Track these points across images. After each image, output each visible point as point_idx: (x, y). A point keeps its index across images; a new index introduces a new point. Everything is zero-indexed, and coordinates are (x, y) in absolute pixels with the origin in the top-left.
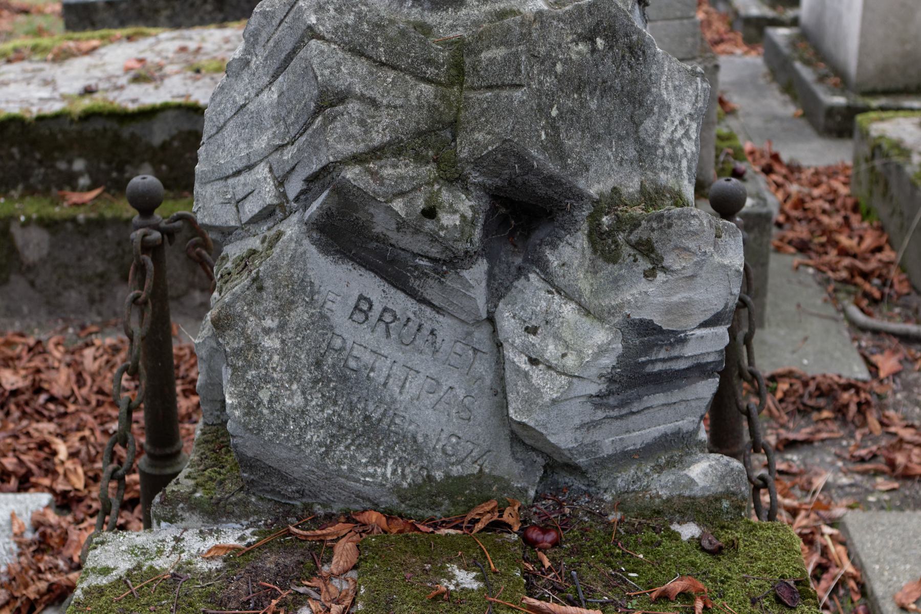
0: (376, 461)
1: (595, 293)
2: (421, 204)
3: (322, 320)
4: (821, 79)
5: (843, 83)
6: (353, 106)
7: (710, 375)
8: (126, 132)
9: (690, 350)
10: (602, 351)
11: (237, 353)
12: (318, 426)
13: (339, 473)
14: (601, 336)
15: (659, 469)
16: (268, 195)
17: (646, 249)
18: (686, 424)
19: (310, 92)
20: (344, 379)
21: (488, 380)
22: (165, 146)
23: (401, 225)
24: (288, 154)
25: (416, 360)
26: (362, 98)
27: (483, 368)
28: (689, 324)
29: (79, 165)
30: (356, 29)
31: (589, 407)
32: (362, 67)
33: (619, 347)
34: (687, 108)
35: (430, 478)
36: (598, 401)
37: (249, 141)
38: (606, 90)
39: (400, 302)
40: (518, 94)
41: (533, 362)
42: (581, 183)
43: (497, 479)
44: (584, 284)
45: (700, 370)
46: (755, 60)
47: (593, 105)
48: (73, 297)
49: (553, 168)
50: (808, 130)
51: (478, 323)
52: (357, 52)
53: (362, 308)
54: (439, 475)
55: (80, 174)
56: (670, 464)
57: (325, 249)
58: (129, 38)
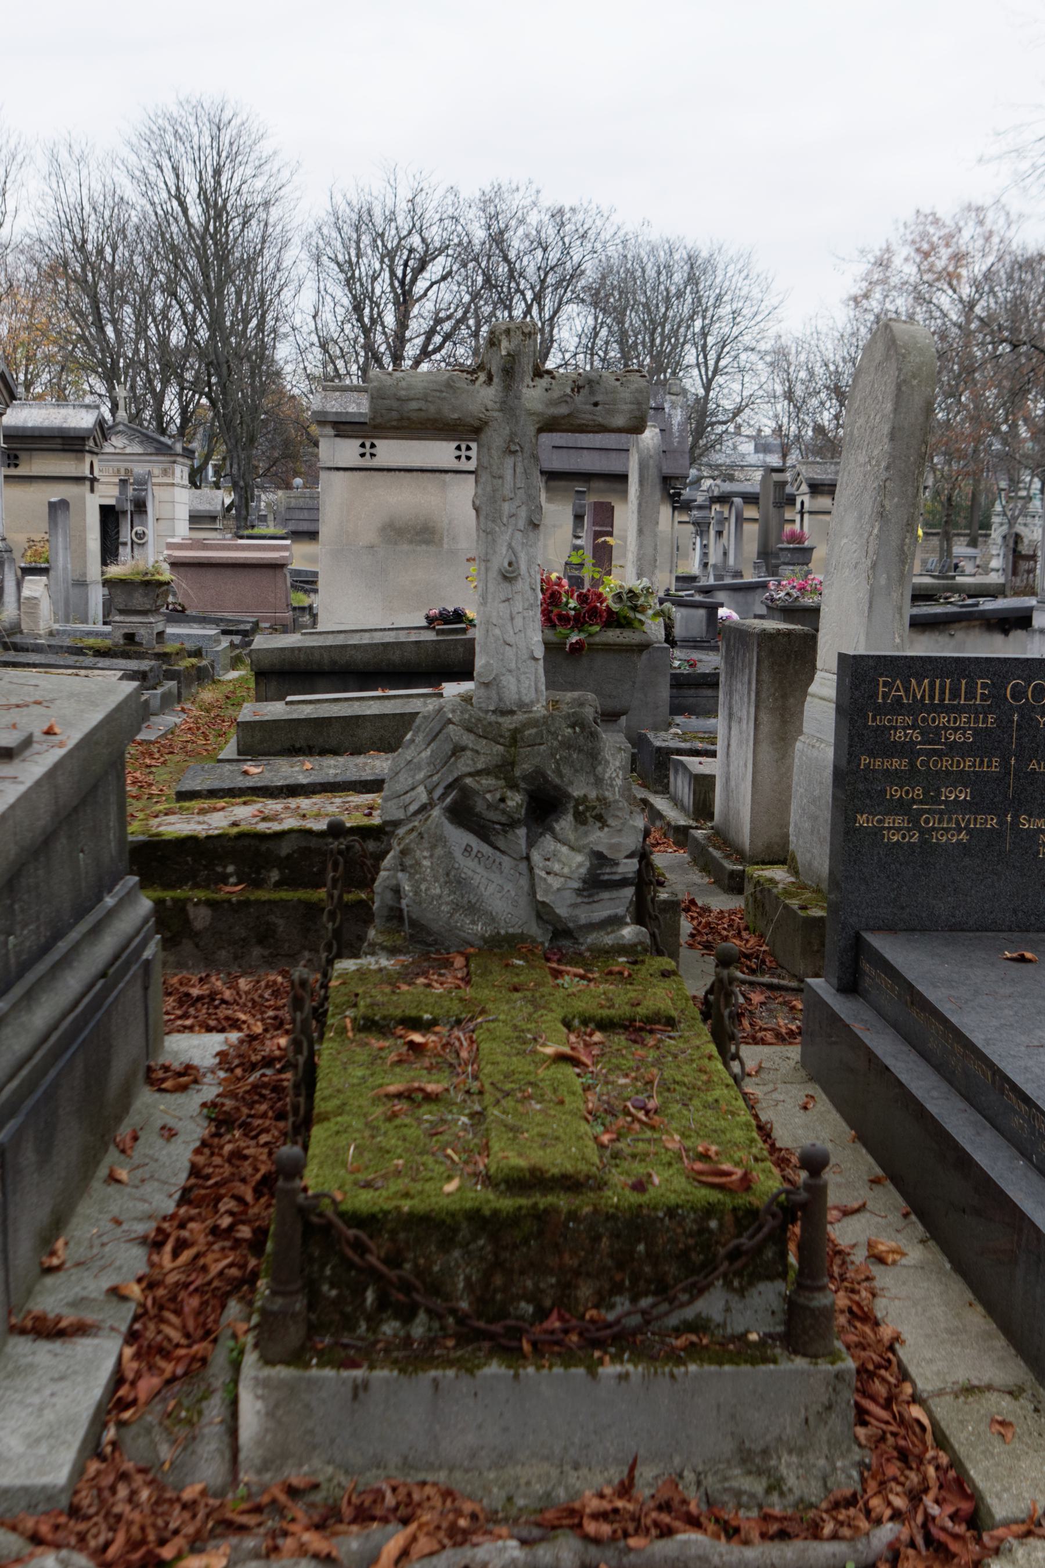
0: (473, 922)
1: (577, 840)
2: (498, 796)
3: (449, 855)
4: (728, 857)
5: (741, 856)
6: (469, 753)
7: (631, 884)
8: (264, 847)
9: (621, 869)
10: (580, 865)
11: (411, 866)
12: (447, 904)
13: (456, 928)
14: (579, 858)
15: (608, 934)
16: (424, 798)
17: (599, 818)
18: (621, 911)
19: (448, 748)
20: (459, 882)
21: (526, 888)
22: (289, 856)
23: (489, 806)
24: (435, 778)
25: (492, 876)
26: (472, 750)
27: (524, 882)
28: (620, 856)
29: (230, 869)
30: (469, 721)
31: (574, 895)
32: (472, 737)
33: (588, 864)
34: (618, 764)
35: (498, 933)
36: (579, 892)
37: (413, 777)
38: (580, 751)
39: (486, 849)
40: (542, 747)
41: (548, 873)
42: (570, 790)
43: (531, 937)
44: (571, 837)
45: (623, 883)
46: (683, 855)
47: (575, 756)
48: (223, 954)
49: (557, 781)
50: (719, 890)
51: (522, 858)
52: (469, 730)
53: (468, 849)
54: (503, 932)
55: (231, 875)
56: (612, 932)
57: (452, 821)
58: (245, 803)
